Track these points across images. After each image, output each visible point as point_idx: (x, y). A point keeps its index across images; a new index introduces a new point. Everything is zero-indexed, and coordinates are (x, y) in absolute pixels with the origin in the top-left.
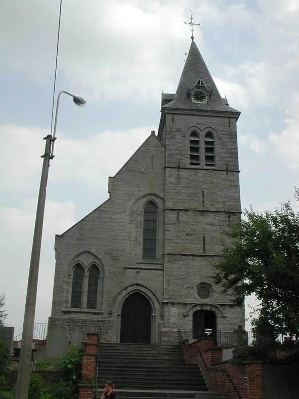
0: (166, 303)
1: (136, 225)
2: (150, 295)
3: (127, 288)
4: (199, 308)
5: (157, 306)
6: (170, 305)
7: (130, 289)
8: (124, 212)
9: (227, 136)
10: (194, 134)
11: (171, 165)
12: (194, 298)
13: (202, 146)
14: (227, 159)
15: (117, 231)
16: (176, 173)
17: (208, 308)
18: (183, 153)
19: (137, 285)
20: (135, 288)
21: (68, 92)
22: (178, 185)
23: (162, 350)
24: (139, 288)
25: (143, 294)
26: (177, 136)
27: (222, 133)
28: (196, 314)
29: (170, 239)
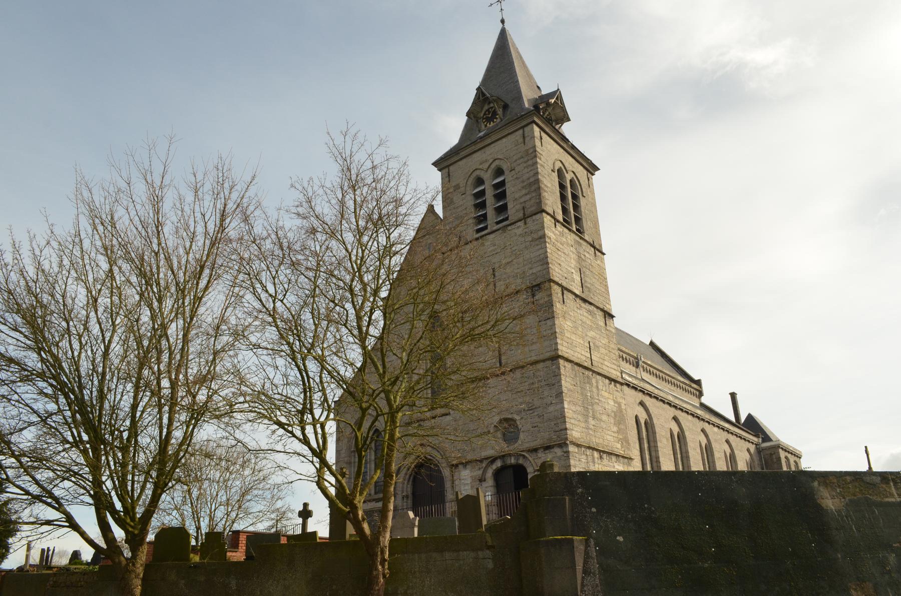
0: (457, 466)
4: (499, 464)
5: (446, 472)
6: (460, 466)
10: (480, 181)
12: (495, 446)
13: (489, 197)
14: (522, 200)
17: (513, 461)
21: (562, 150)
23: (147, 416)
26: (455, 198)
28: (497, 474)
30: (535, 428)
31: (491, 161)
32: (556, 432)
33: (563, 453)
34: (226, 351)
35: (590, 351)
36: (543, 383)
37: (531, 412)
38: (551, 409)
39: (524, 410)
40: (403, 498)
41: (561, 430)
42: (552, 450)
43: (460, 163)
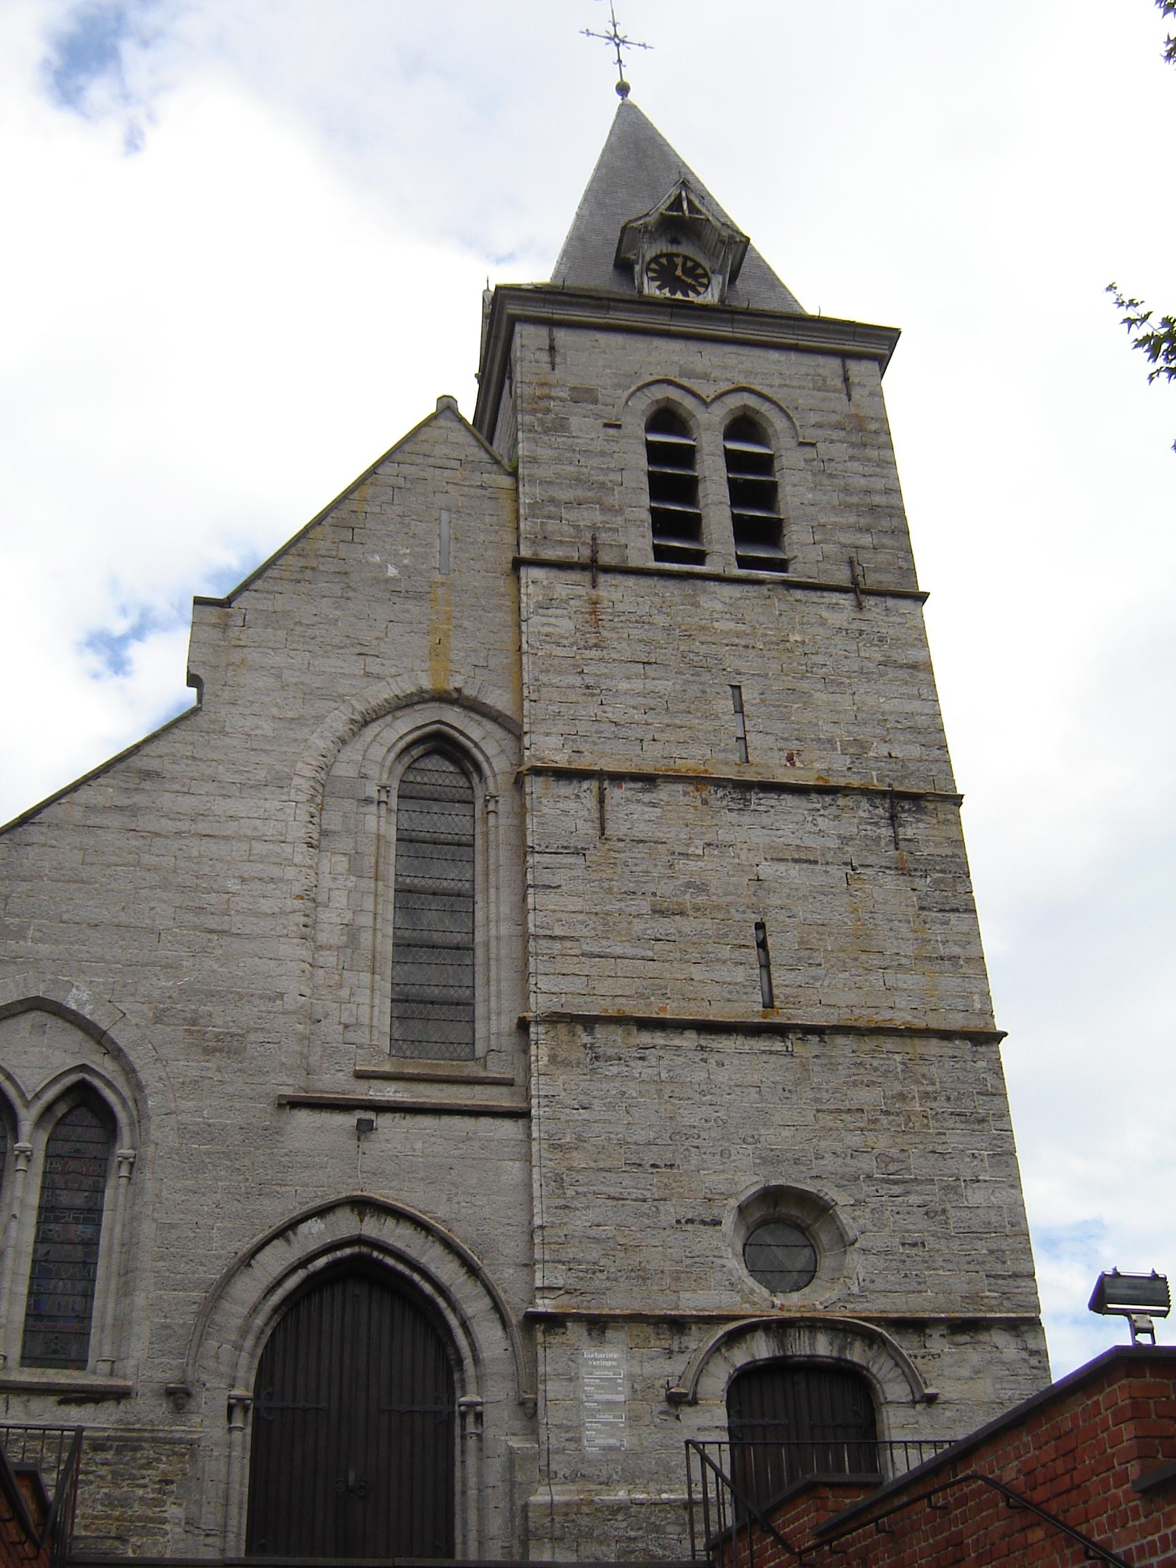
0: (554, 1322)
1: (355, 858)
2: (447, 1270)
3: (293, 1225)
4: (761, 1348)
7: (315, 1233)
8: (280, 782)
9: (842, 433)
11: (549, 554)
15: (233, 885)
16: (581, 591)
18: (614, 499)
19: (362, 1205)
20: (346, 1224)
22: (594, 653)
24: (372, 1227)
25: (401, 1267)
27: (814, 418)
29: (558, 931)
30: (914, 1251)
31: (725, 386)
32: (996, 1277)
33: (1025, 1355)
34: (642, 1375)
35: (551, 887)
36: (940, 1105)
37: (896, 1189)
38: (976, 1196)
39: (869, 1177)
40: (231, 1408)
41: (1015, 1276)
42: (984, 1337)
43: (602, 338)
